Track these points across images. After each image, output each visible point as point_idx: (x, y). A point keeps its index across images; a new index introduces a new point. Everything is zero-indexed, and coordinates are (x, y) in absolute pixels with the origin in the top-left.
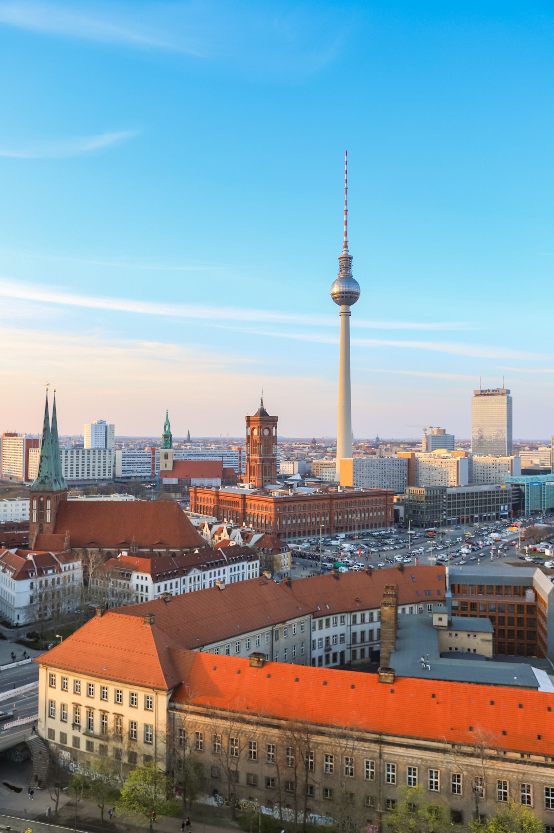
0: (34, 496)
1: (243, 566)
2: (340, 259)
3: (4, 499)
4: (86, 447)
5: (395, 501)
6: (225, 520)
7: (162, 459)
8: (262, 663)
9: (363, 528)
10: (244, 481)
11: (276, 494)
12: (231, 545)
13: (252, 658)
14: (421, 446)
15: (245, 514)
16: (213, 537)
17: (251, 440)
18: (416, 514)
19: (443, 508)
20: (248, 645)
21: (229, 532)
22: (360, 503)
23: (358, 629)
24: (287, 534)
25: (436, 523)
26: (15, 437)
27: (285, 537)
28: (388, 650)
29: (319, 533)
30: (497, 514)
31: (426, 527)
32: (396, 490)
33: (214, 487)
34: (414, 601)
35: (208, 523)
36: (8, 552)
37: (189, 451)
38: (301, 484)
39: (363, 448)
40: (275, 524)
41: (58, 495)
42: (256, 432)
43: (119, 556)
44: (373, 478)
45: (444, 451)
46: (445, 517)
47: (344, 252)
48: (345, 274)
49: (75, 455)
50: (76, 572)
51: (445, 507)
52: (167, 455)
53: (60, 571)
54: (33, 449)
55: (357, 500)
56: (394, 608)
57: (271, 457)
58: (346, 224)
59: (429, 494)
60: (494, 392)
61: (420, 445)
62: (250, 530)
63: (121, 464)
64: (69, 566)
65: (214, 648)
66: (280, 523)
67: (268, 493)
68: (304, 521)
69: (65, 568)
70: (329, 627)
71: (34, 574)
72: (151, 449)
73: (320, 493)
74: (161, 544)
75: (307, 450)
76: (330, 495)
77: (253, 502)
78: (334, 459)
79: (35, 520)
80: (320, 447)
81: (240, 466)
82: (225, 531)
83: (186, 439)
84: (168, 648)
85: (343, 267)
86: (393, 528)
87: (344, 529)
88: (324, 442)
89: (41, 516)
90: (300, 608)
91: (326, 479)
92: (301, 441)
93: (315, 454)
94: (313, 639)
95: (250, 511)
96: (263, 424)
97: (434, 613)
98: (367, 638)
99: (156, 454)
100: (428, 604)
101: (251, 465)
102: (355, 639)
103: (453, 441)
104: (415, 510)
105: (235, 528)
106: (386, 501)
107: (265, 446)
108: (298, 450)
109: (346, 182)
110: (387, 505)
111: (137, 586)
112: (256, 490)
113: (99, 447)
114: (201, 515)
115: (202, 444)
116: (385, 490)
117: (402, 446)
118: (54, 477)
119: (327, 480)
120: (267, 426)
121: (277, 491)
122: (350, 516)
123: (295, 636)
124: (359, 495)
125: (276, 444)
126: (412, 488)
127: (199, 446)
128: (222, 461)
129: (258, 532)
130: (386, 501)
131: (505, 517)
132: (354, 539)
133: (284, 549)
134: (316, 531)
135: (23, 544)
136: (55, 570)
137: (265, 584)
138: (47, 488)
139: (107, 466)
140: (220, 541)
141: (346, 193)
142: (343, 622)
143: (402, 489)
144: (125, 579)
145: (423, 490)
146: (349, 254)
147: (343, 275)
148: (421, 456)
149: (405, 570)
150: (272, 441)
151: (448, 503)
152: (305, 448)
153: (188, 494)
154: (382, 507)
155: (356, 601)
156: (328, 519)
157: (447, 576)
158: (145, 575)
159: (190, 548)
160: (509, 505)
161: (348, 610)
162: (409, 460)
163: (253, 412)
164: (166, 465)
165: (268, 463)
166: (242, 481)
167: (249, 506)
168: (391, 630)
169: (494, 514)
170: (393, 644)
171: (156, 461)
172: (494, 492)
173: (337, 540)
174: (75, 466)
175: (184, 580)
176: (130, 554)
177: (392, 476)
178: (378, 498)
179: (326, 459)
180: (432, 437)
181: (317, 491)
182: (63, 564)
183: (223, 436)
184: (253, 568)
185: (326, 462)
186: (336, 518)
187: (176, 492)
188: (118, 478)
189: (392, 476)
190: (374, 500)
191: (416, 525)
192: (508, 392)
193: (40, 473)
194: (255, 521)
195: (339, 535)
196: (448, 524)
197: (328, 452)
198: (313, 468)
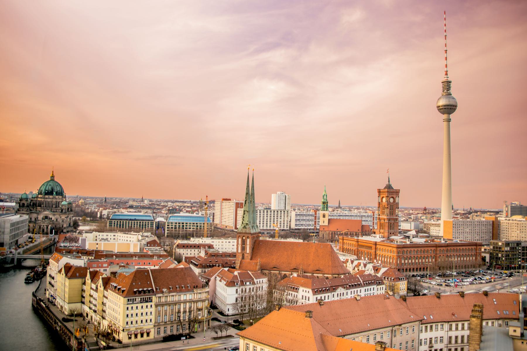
0: (239, 236)
1: (374, 288)
2: (442, 83)
3: (222, 238)
4: (273, 208)
5: (483, 250)
6: (362, 258)
7: (321, 218)
8: (383, 349)
10: (376, 233)
12: (366, 274)
13: (377, 345)
14: (503, 214)
16: (354, 269)
20: (375, 338)
21: (365, 265)
22: (457, 250)
23: (453, 334)
25: (513, 267)
26: (229, 201)
28: (474, 349)
34: (495, 318)
35: (351, 259)
36: (223, 269)
41: (254, 236)
42: (384, 200)
43: (291, 277)
45: (521, 216)
46: (520, 263)
47: (446, 78)
48: (446, 93)
49: (265, 214)
50: (264, 284)
51: (520, 255)
52: (325, 215)
53: (254, 283)
54: (240, 209)
55: (455, 248)
56: (479, 320)
61: (502, 213)
62: (379, 265)
63: (295, 220)
64: (260, 281)
65: (351, 338)
66: (400, 261)
69: (257, 281)
70: (432, 331)
71: (238, 284)
74: (318, 271)
76: (436, 244)
77: (381, 247)
78: (439, 221)
79: (240, 251)
81: (373, 224)
82: (362, 265)
84: (321, 334)
89: (243, 249)
90: (412, 317)
91: (433, 234)
94: (420, 338)
96: (390, 194)
97: (510, 326)
98: (459, 341)
99: (317, 214)
100: (505, 321)
102: (451, 341)
106: (476, 249)
107: (390, 209)
108: (414, 214)
109: (445, 32)
110: (476, 252)
111: (303, 296)
112: (384, 239)
113: (281, 209)
114: (346, 254)
115: (348, 210)
116: (476, 242)
117: (489, 213)
118: (252, 224)
119: (434, 235)
120: (392, 196)
121: (398, 239)
123: (408, 335)
127: (346, 211)
129: (384, 267)
133: (402, 279)
134: (425, 268)
135: (232, 266)
136: (251, 283)
137: (388, 298)
138: (248, 231)
139: (286, 221)
141: (446, 39)
142: (442, 328)
143: (488, 242)
144: (295, 292)
146: (449, 80)
148: (502, 219)
149: (488, 295)
150: (395, 206)
151: (522, 253)
154: (473, 254)
155: (452, 314)
157: (521, 301)
158: (307, 290)
159: (338, 275)
161: (446, 321)
163: (382, 187)
164: (324, 221)
165: (392, 221)
166: (375, 233)
168: (477, 335)
170: (479, 345)
174: (265, 221)
175: (333, 295)
176: (298, 276)
178: (470, 247)
182: (256, 279)
184: (380, 290)
185: (433, 223)
188: (293, 229)
190: (467, 249)
193: (244, 222)
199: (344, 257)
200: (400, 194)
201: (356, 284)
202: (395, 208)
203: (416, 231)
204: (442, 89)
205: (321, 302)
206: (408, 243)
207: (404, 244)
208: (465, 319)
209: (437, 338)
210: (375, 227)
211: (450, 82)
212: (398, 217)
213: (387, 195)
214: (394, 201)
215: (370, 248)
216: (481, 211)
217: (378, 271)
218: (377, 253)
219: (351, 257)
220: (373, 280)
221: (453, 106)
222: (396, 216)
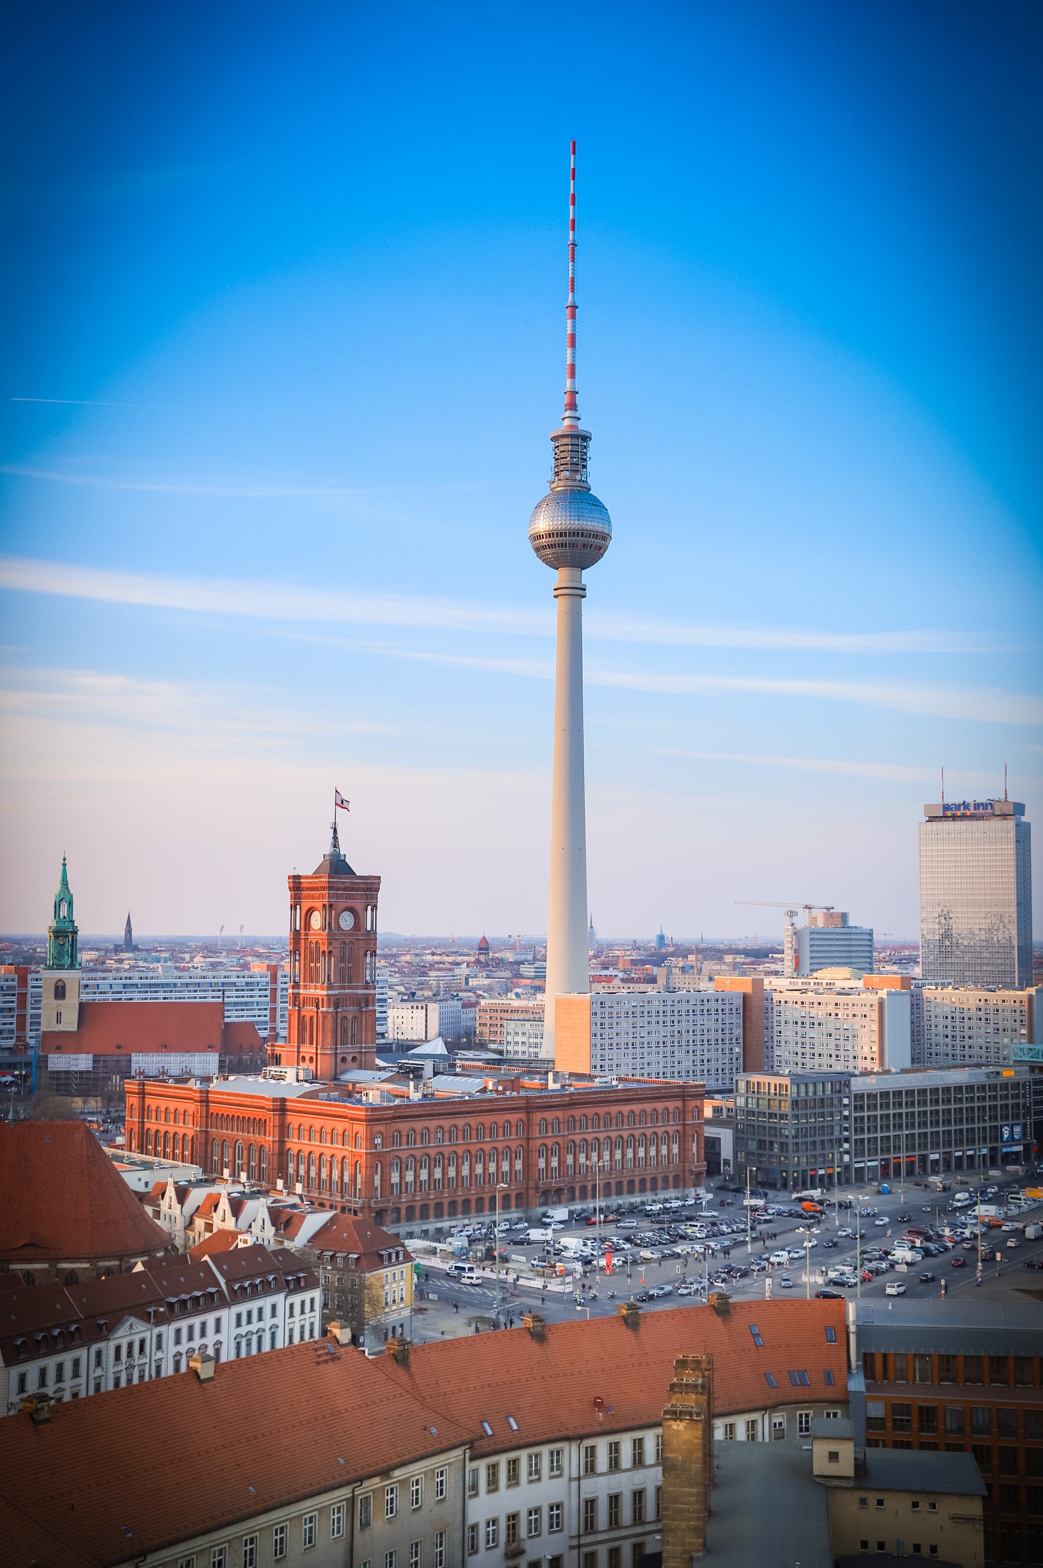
2: (554, 439)
5: (708, 1113)
6: (226, 1172)
9: (619, 1193)
10: (283, 1060)
11: (373, 1097)
12: (241, 1245)
15: (283, 1154)
17: (303, 942)
18: (767, 1152)
19: (841, 1133)
21: (236, 1207)
22: (609, 1121)
23: (600, 1487)
24: (403, 1212)
27: (398, 1220)
28: (684, 1552)
29: (492, 1209)
30: (992, 1149)
31: (795, 1189)
32: (711, 1084)
33: (196, 1077)
34: (760, 1404)
35: (176, 1183)
37: (126, 974)
38: (446, 1066)
39: (620, 966)
40: (369, 1181)
45: (845, 972)
46: (846, 1158)
47: (567, 422)
48: (570, 483)
51: (846, 1129)
52: (64, 987)
55: (602, 1110)
57: (360, 992)
58: (573, 345)
59: (803, 1094)
61: (779, 956)
67: (349, 1093)
68: (452, 1172)
70: (518, 1484)
72: (17, 971)
73: (497, 1091)
75: (463, 971)
77: (307, 1121)
78: (539, 996)
80: (500, 963)
81: (273, 1019)
82: (224, 1205)
83: (121, 942)
85: (563, 461)
86: (701, 1191)
87: (564, 1197)
88: (512, 948)
92: (450, 947)
93: (487, 982)
96: (338, 897)
97: (816, 1438)
98: (626, 1514)
99: (31, 983)
101: (303, 1013)
105: (254, 1195)
106: (683, 1113)
107: (342, 959)
110: (684, 1125)
112: (317, 1086)
116: (681, 1082)
117: (729, 958)
119: (520, 1056)
120: (350, 903)
122: (582, 1159)
123: (419, 1513)
124: (607, 1098)
125: (374, 954)
126: (755, 1078)
128: (223, 1003)
130: (683, 1113)
131: (1010, 1158)
132: (594, 1223)
133: (394, 1256)
137: (333, 1360)
140: (208, 1235)
143: (727, 1081)
145: (787, 1081)
147: (562, 483)
150: (362, 944)
151: (856, 1119)
152: (458, 964)
153: (122, 1097)
154: (671, 1130)
156: (519, 1165)
157: (852, 1328)
159: (120, 1258)
160: (1024, 1126)
161: (570, 1434)
162: (745, 997)
166: (277, 1060)
168: (694, 1490)
169: (985, 1151)
170: (700, 1532)
171: (29, 1006)
172: (982, 1088)
173: (546, 1225)
178: (660, 1106)
179: (517, 995)
180: (811, 933)
183: (226, 933)
185: (516, 1003)
186: (542, 1164)
187: (85, 1094)
191: (766, 1184)
194: (313, 1174)
195: (550, 1212)
196: (854, 1178)
197: (522, 977)
198: (478, 1020)
199: (146, 1175)
200: (380, 895)
201: (198, 1294)
202: (362, 951)
203: (446, 1043)
204: (553, 462)
205: (37, 1410)
206: (416, 1097)
207: (397, 1102)
208: (645, 1421)
209: (537, 1510)
210: (278, 1030)
211: (586, 438)
212: (372, 992)
214: (358, 924)
215: (260, 1124)
216: (699, 951)
217: (291, 1228)
218: (288, 1145)
219: (174, 1171)
220: (270, 1272)
221: (596, 536)
222: (367, 987)
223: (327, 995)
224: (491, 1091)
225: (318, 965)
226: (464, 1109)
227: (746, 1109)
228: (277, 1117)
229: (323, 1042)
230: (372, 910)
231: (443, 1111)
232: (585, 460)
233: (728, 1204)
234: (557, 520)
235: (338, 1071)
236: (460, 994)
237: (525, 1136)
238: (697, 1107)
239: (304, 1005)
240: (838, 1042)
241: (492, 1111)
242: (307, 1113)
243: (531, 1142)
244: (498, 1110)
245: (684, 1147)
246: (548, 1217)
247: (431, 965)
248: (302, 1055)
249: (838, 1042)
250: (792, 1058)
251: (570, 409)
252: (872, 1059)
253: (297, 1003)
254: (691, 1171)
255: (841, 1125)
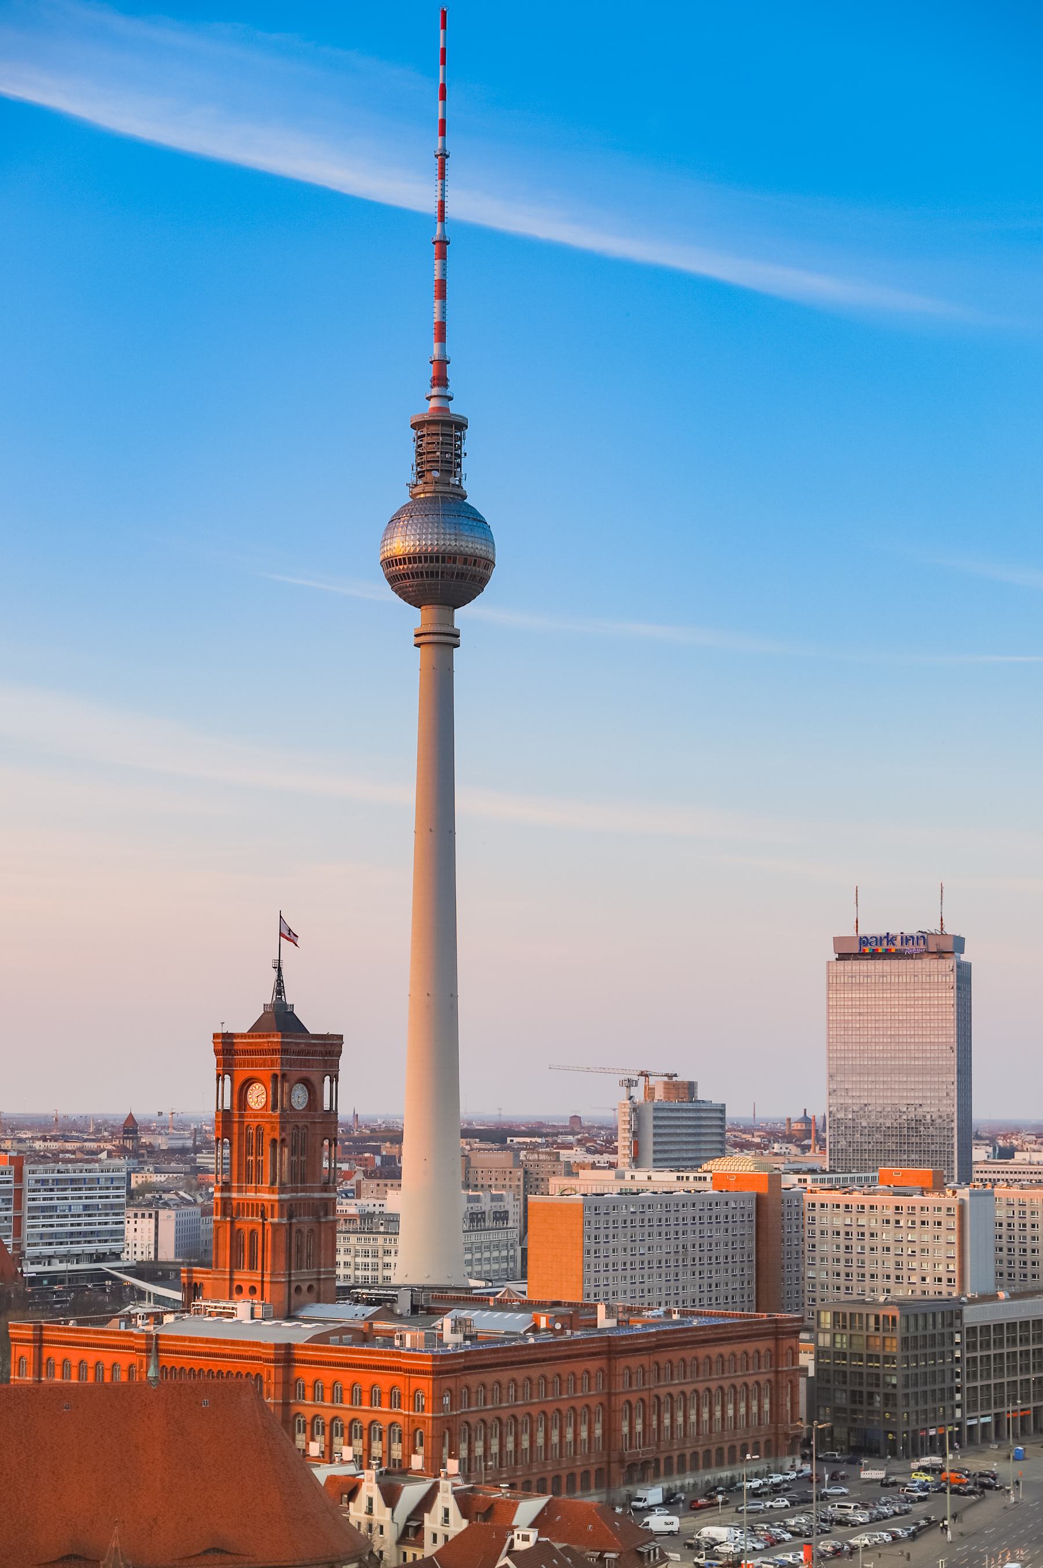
17: (236, 1126)
18: (865, 1407)
19: (953, 1380)
42: (257, 1097)
44: (714, 1267)
47: (434, 403)
48: (440, 488)
51: (958, 1375)
57: (316, 1195)
60: (909, 948)
73: (553, 1330)
77: (327, 1376)
85: (430, 457)
95: (353, 1415)
96: (291, 1063)
101: (238, 1226)
103: (722, 1127)
104: (857, 1388)
106: (775, 1357)
107: (293, 1152)
110: (777, 1372)
120: (304, 1072)
125: (334, 1141)
147: (429, 488)
163: (241, 1024)
165: (306, 1218)
167: (309, 1392)
177: (706, 1261)
178: (750, 1347)
180: (655, 1110)
181: (543, 1323)
189: (706, 1261)
190: (739, 1354)
192: (959, 943)
195: (640, 1494)
204: (412, 458)
211: (461, 425)
212: (333, 1195)
213: (277, 1069)
222: (325, 1189)
223: (279, 1201)
224: (545, 1330)
225: (260, 1158)
226: (540, 1356)
227: (832, 1350)
228: (281, 1370)
229: (273, 1265)
230: (331, 1082)
231: (517, 1359)
232: (460, 457)
233: (843, 1477)
234: (426, 539)
235: (292, 1306)
236: (164, 1196)
237: (606, 1391)
238: (791, 1348)
239: (238, 1214)
240: (899, 1259)
241: (569, 1357)
242: (329, 1364)
243: (613, 1398)
244: (576, 1356)
245: (777, 1402)
246: (639, 1500)
247: (53, 1155)
248: (236, 1284)
249: (899, 1259)
250: (832, 1280)
251: (439, 385)
252: (950, 1280)
253: (229, 1211)
254: (786, 1435)
255: (952, 1370)
